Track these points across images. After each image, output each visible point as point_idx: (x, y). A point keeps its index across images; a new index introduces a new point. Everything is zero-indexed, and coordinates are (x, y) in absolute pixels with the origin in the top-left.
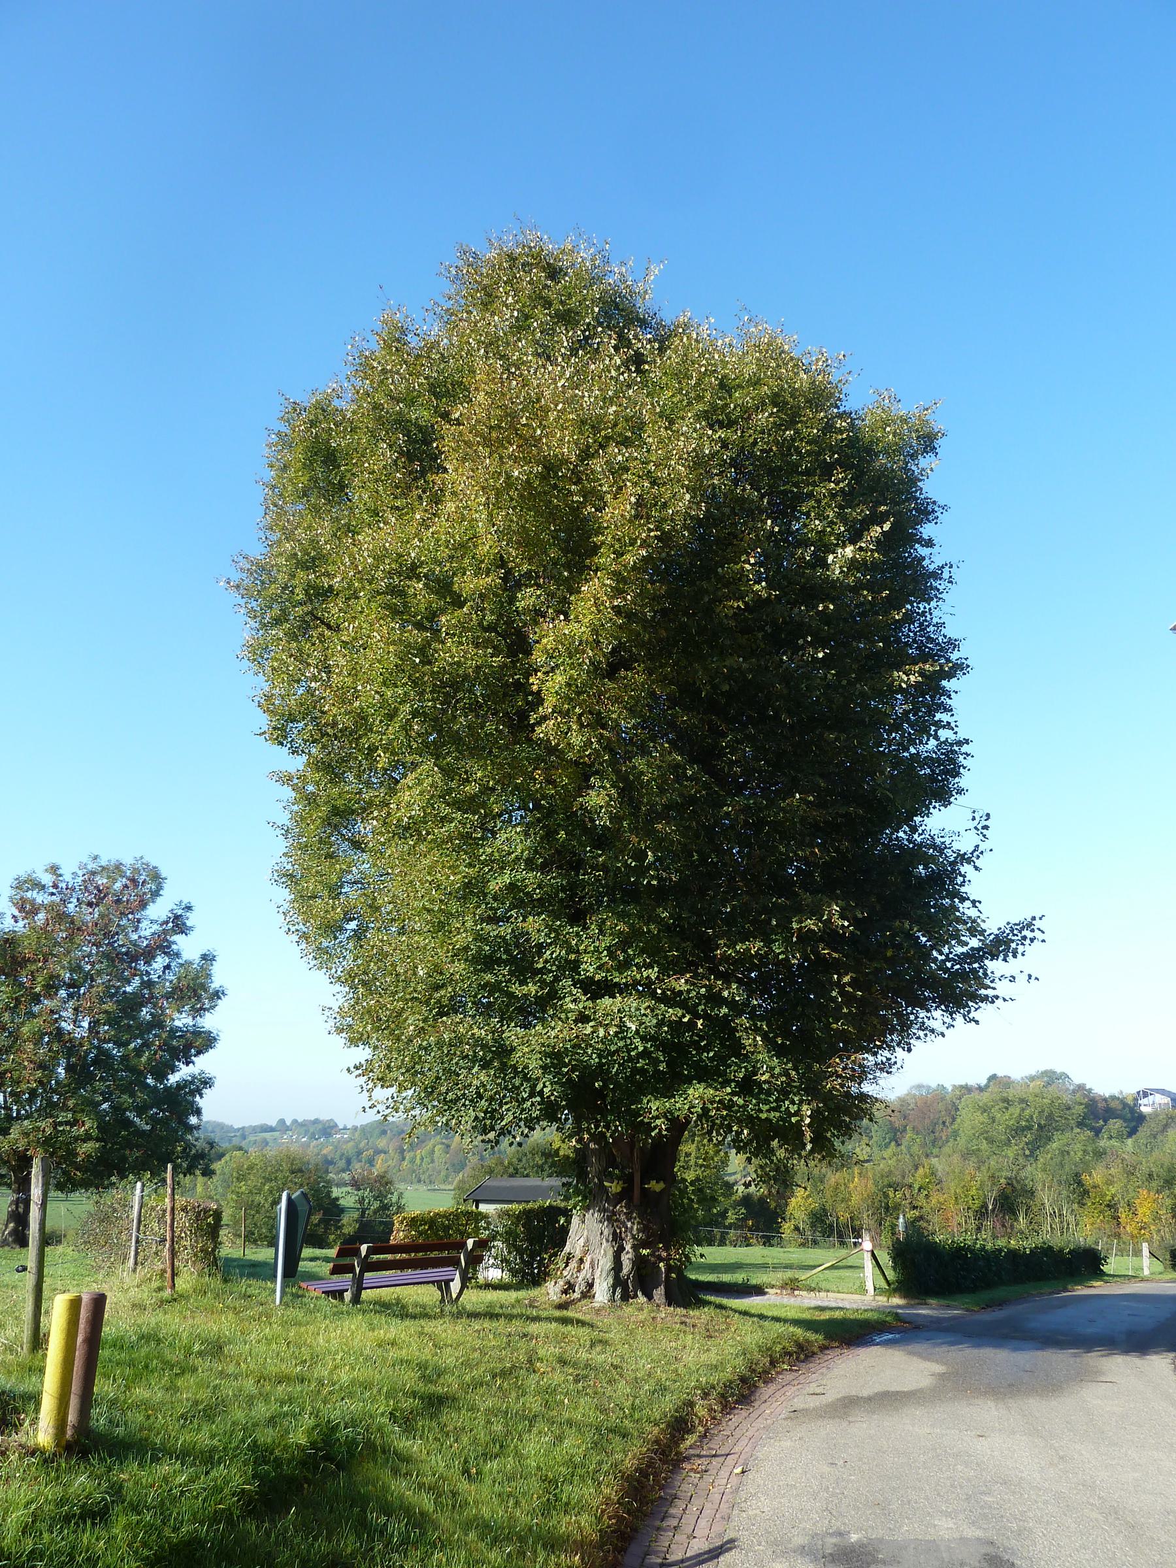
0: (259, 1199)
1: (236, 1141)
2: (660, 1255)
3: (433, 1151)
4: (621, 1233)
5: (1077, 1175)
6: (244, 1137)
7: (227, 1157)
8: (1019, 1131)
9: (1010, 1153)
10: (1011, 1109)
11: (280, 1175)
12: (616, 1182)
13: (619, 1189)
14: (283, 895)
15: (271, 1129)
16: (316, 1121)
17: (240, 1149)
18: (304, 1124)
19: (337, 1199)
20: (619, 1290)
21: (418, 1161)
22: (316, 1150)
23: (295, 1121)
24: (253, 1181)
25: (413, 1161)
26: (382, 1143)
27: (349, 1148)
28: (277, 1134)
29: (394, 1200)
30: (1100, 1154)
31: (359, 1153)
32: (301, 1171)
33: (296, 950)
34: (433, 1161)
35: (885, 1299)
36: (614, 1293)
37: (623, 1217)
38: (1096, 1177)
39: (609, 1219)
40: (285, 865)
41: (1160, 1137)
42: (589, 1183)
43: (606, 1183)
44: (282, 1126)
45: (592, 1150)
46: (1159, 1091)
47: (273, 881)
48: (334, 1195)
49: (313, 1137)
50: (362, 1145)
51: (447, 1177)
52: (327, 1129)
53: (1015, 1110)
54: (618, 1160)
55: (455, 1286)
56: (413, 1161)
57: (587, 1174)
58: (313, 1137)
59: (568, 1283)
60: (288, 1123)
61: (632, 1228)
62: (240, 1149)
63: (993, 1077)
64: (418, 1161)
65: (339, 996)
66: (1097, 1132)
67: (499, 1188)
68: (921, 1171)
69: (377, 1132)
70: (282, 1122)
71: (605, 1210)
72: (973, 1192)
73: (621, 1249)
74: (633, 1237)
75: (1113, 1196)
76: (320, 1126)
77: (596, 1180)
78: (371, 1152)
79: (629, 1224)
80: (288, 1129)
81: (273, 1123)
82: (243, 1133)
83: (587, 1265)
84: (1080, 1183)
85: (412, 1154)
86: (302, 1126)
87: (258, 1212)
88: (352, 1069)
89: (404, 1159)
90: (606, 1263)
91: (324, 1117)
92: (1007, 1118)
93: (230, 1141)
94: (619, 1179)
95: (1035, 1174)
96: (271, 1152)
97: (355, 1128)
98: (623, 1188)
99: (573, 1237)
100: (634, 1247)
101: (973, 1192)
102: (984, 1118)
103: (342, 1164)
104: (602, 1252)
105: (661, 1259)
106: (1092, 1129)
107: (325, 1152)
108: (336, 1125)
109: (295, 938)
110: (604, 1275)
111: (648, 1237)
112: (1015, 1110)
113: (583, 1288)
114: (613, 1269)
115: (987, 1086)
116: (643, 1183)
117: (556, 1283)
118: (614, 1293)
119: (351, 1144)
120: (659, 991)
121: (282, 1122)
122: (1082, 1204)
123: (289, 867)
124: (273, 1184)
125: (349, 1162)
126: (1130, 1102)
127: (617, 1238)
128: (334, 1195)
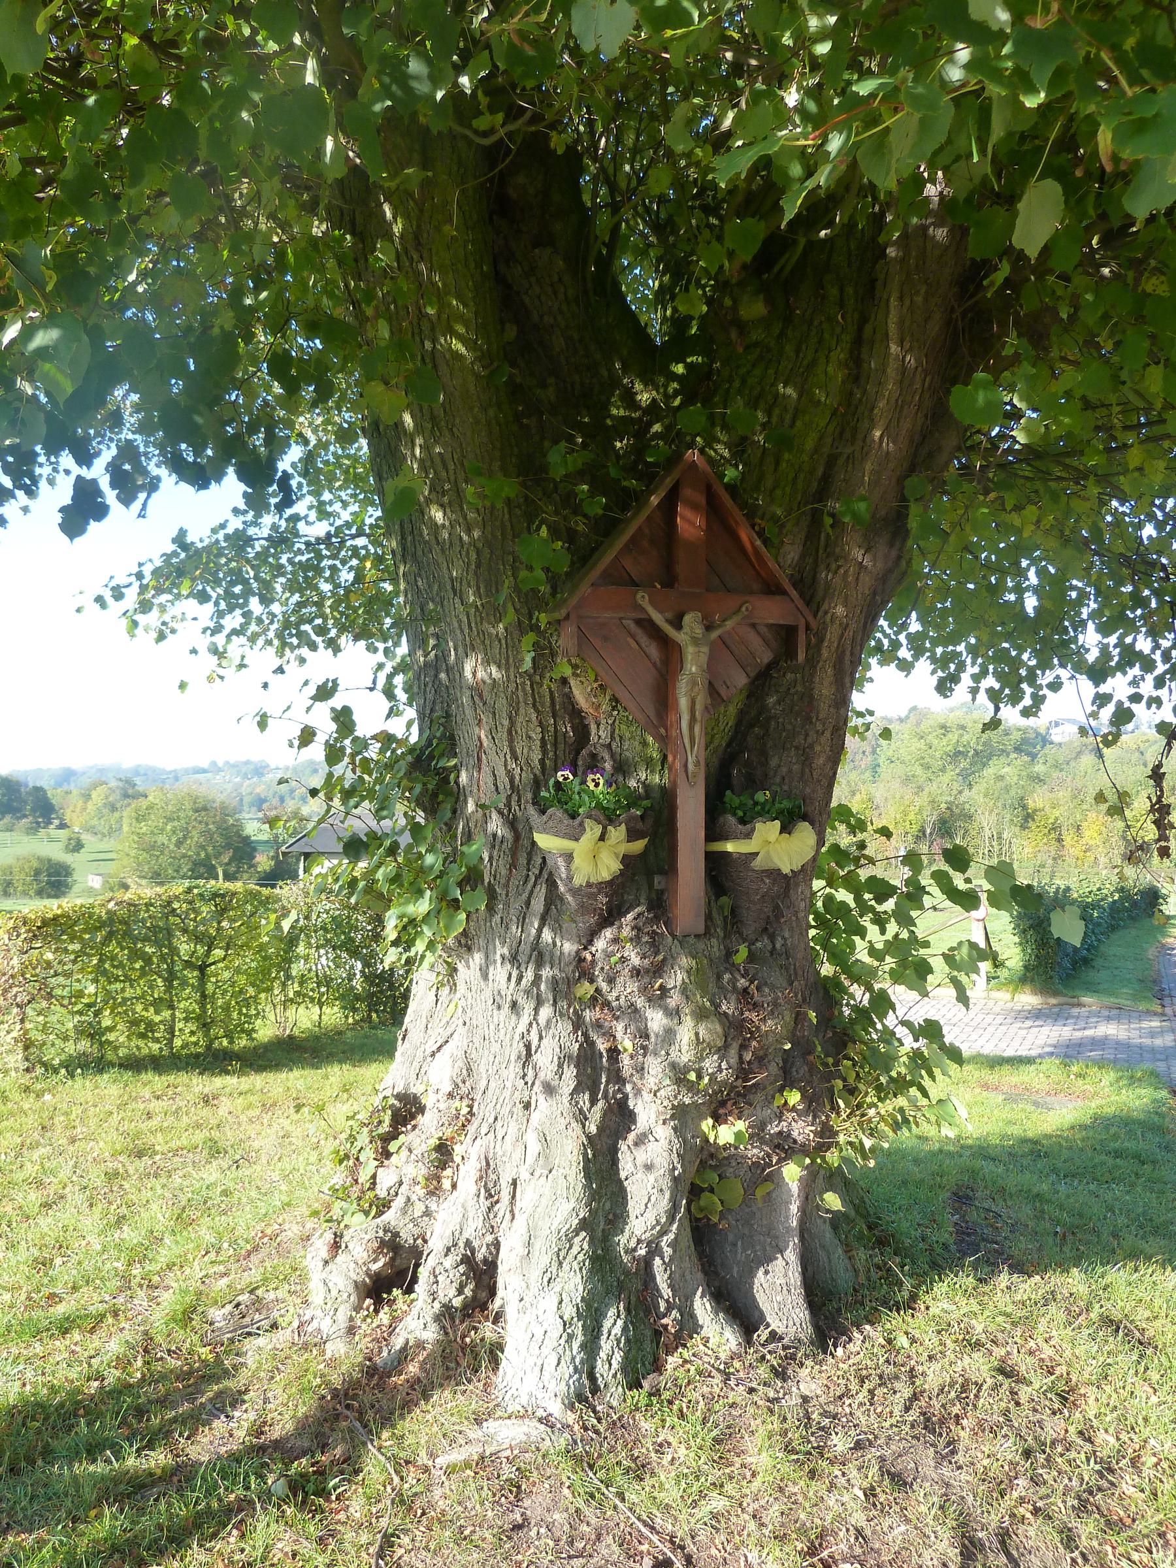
0: (162, 839)
2: (784, 1136)
4: (614, 1053)
5: (1022, 799)
6: (177, 779)
8: (957, 755)
9: (946, 778)
10: (950, 736)
11: (182, 815)
12: (592, 830)
13: (609, 867)
15: (204, 771)
16: (247, 763)
18: (234, 766)
20: (614, 1324)
23: (227, 763)
24: (154, 821)
28: (209, 775)
30: (1038, 779)
32: (205, 809)
35: (1008, 996)
36: (591, 1347)
37: (626, 990)
38: (1037, 800)
39: (562, 990)
41: (1073, 764)
42: (468, 837)
43: (544, 841)
44: (215, 768)
45: (477, 691)
46: (1069, 721)
49: (245, 777)
52: (259, 770)
53: (953, 737)
54: (599, 734)
57: (458, 796)
58: (245, 777)
59: (391, 1244)
60: (220, 764)
61: (669, 1036)
63: (914, 708)
66: (1033, 756)
68: (858, 797)
70: (214, 763)
71: (539, 955)
72: (912, 816)
74: (679, 1075)
75: (1057, 819)
77: (495, 825)
79: (656, 1020)
80: (220, 770)
81: (205, 765)
83: (467, 1174)
84: (1024, 807)
87: (162, 852)
91: (255, 758)
92: (945, 745)
94: (608, 817)
95: (976, 798)
98: (626, 860)
100: (682, 1117)
101: (912, 816)
102: (921, 744)
104: (534, 1146)
105: (785, 1147)
106: (1028, 754)
107: (258, 790)
110: (543, 1258)
111: (743, 1072)
112: (953, 737)
113: (448, 1292)
114: (584, 1225)
115: (907, 717)
118: (591, 1347)
121: (214, 763)
122: (1023, 827)
124: (176, 823)
126: (1043, 731)
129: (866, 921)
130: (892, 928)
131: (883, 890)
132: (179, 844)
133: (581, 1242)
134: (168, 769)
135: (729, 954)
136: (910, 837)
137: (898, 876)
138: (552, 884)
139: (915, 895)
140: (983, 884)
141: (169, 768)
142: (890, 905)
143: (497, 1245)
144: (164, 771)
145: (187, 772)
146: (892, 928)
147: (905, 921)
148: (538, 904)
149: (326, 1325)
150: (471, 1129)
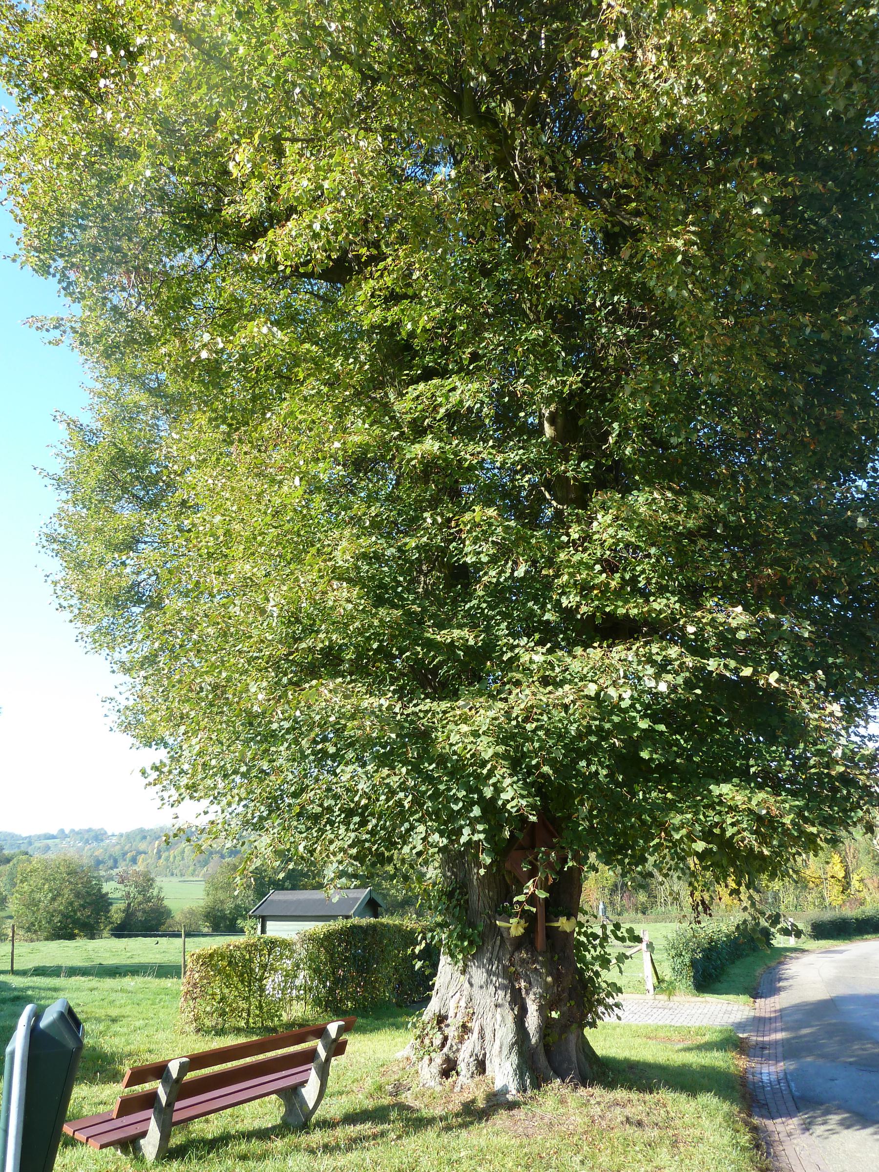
1: (23, 849)
3: (183, 852)
6: (30, 843)
7: (15, 861)
13: (521, 931)
14: (55, 566)
15: (54, 837)
16: (90, 830)
17: (27, 853)
18: (78, 833)
19: (107, 894)
21: (171, 859)
22: (89, 854)
23: (73, 831)
25: (167, 859)
26: (142, 846)
27: (117, 850)
28: (57, 841)
29: (155, 894)
31: (124, 854)
33: (72, 631)
34: (183, 859)
40: (57, 527)
44: (62, 835)
47: (40, 547)
48: (104, 891)
50: (126, 848)
51: (194, 871)
52: (98, 836)
55: (310, 1093)
56: (167, 859)
60: (67, 832)
62: (27, 853)
64: (171, 859)
65: (122, 689)
67: (285, 902)
69: (138, 838)
70: (62, 831)
73: (523, 1011)
76: (93, 834)
78: (134, 853)
80: (66, 836)
81: (54, 832)
82: (30, 841)
85: (166, 854)
86: (77, 834)
88: (149, 771)
89: (160, 858)
90: (506, 1033)
91: (96, 826)
93: (19, 847)
96: (51, 855)
97: (121, 836)
99: (442, 991)
100: (541, 1009)
103: (110, 863)
107: (96, 853)
108: (106, 833)
109: (67, 615)
110: (505, 1051)
114: (516, 1043)
116: (548, 920)
117: (431, 1060)
119: (118, 847)
120: (691, 629)
121: (62, 831)
123: (62, 530)
125: (116, 861)
127: (518, 1002)
128: (104, 891)
129: (590, 947)
130: (599, 949)
131: (595, 936)
132: (53, 899)
133: (516, 1048)
134: (24, 835)
135: (553, 957)
136: (606, 891)
137: (599, 932)
138: (502, 937)
139: (605, 938)
140: (626, 935)
141: (25, 834)
142: (597, 942)
143: (485, 1055)
144: (20, 838)
145: (39, 838)
146: (599, 949)
147: (603, 947)
148: (498, 942)
149: (433, 1084)
150: (475, 1017)
